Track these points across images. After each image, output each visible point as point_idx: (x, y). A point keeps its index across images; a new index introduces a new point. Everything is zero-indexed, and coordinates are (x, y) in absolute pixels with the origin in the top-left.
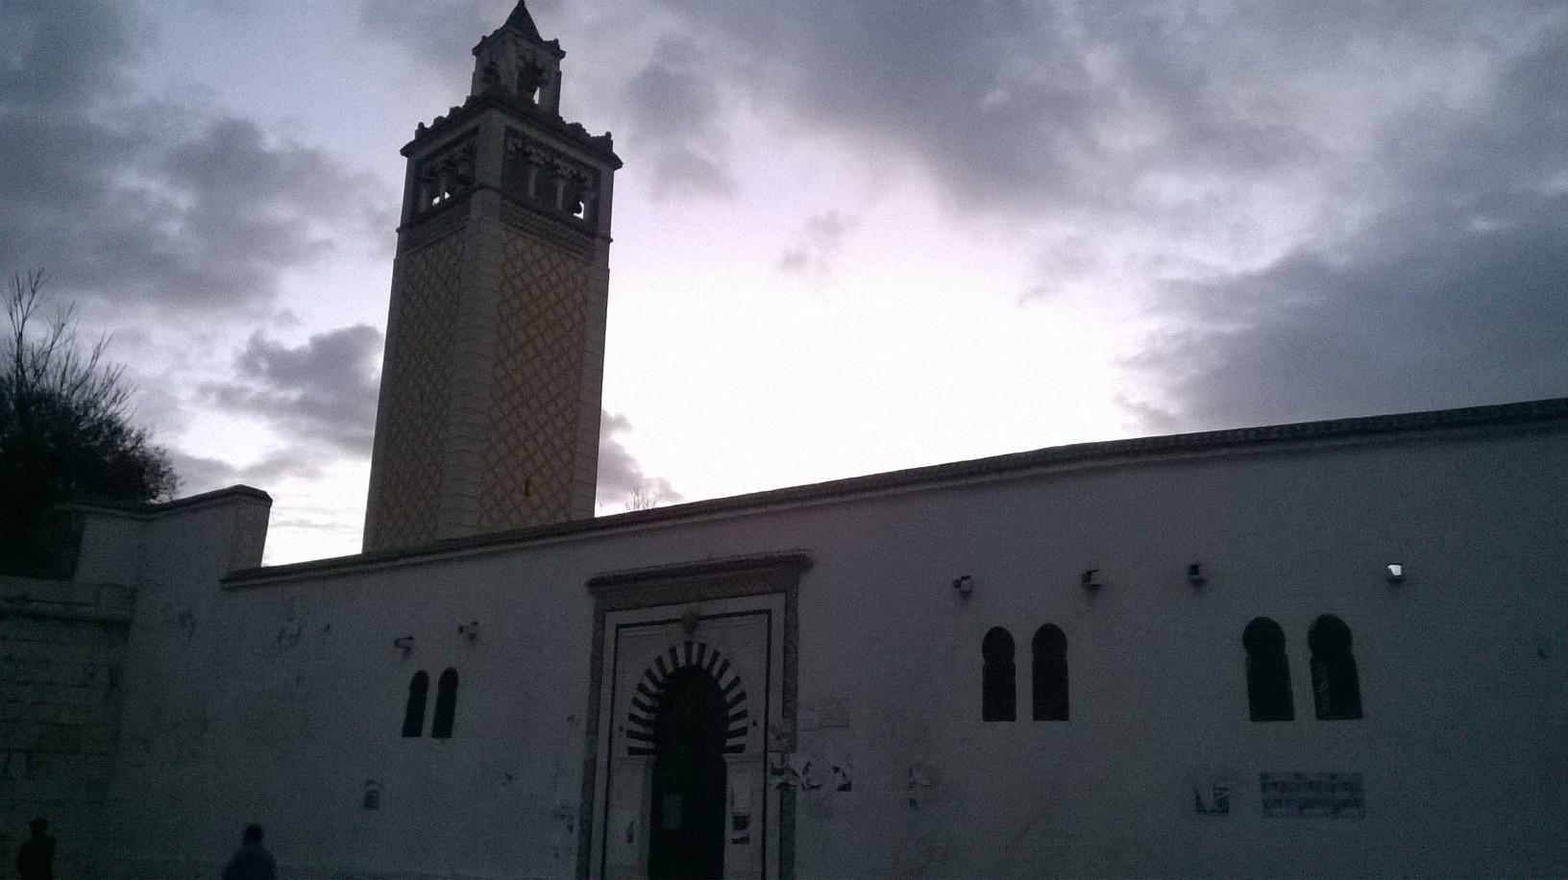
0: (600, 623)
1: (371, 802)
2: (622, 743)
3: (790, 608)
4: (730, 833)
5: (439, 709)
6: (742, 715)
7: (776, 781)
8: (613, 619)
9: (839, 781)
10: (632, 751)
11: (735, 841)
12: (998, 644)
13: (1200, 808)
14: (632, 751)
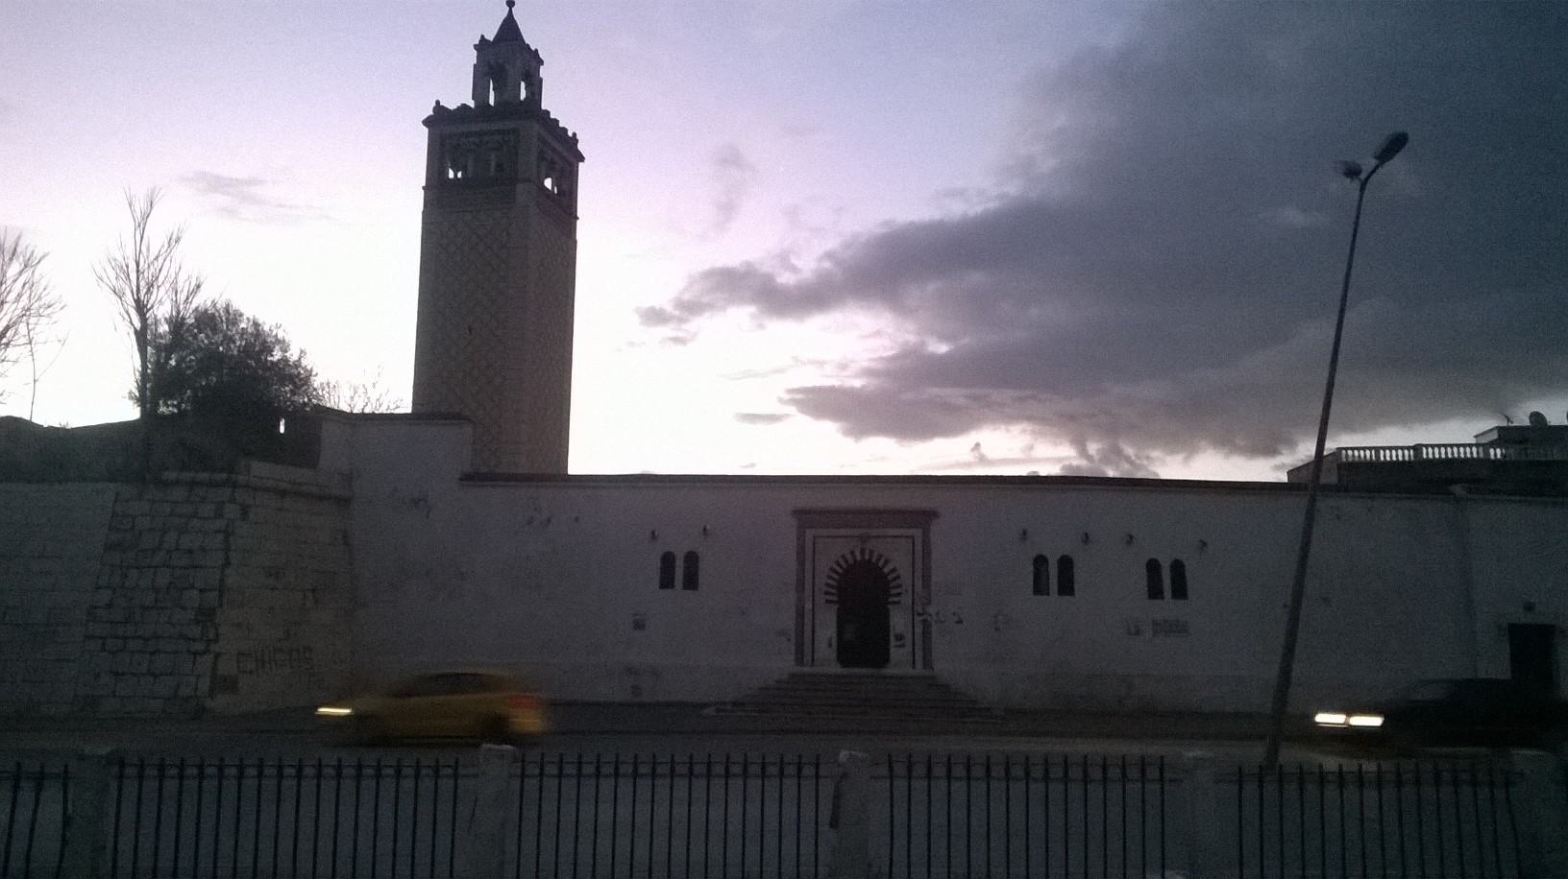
0: (801, 537)
1: (639, 625)
2: (821, 599)
3: (926, 534)
4: (893, 641)
5: (1173, 581)
6: (899, 586)
7: (918, 619)
8: (809, 534)
9: (956, 619)
10: (827, 601)
11: (896, 646)
12: (1040, 561)
13: (1129, 633)
14: (827, 601)
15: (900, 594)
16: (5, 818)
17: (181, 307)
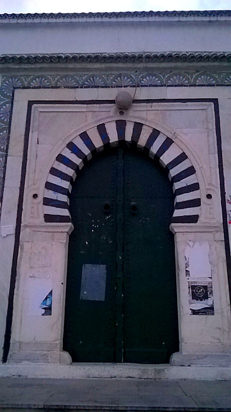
10: (49, 218)
14: (49, 218)
15: (196, 203)
16: (107, 411)
17: (35, 182)
